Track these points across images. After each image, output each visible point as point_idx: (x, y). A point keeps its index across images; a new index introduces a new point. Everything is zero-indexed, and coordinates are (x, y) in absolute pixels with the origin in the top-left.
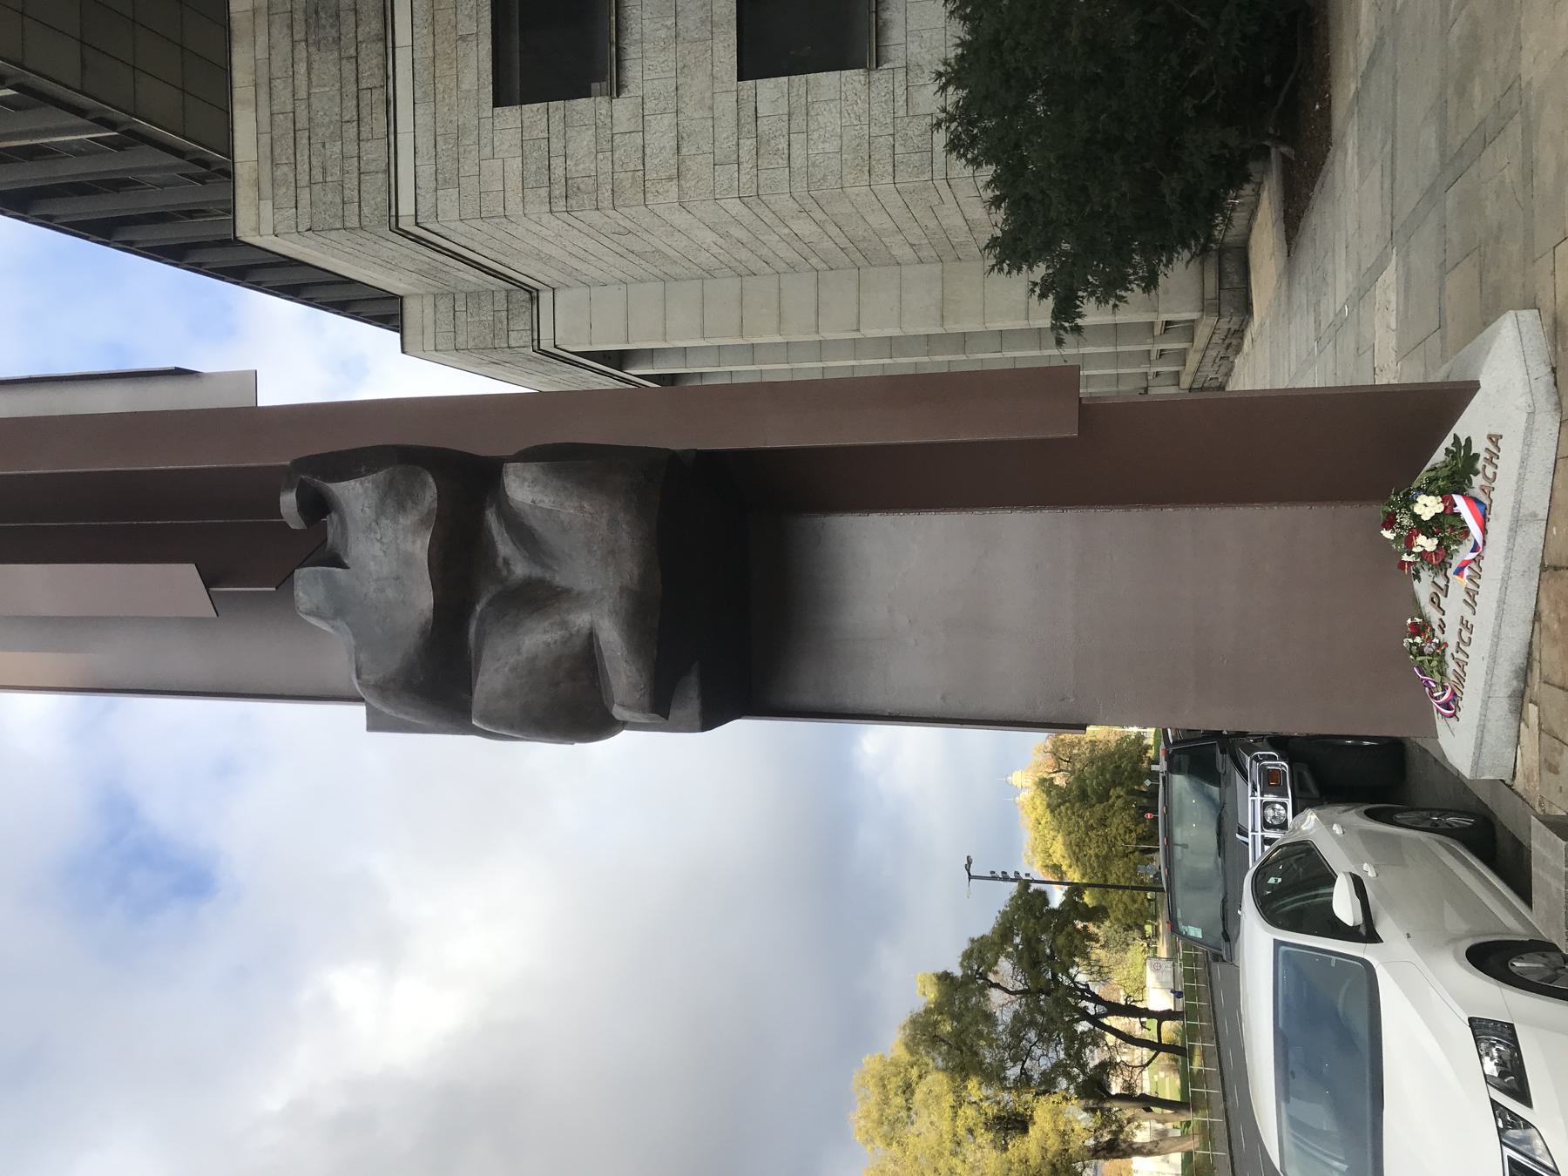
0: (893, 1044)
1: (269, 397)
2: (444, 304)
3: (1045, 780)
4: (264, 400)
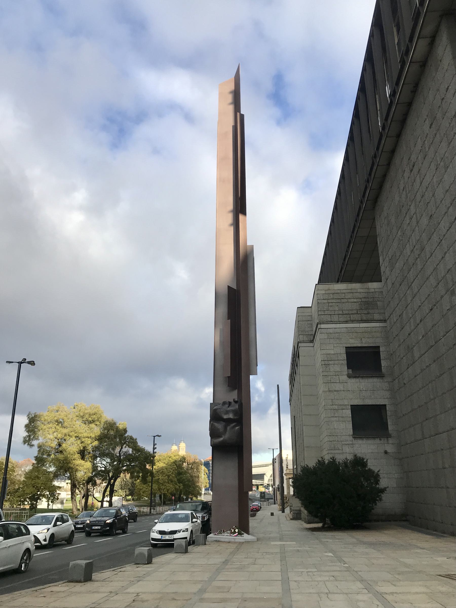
0: (108, 415)
2: (309, 318)
3: (185, 460)
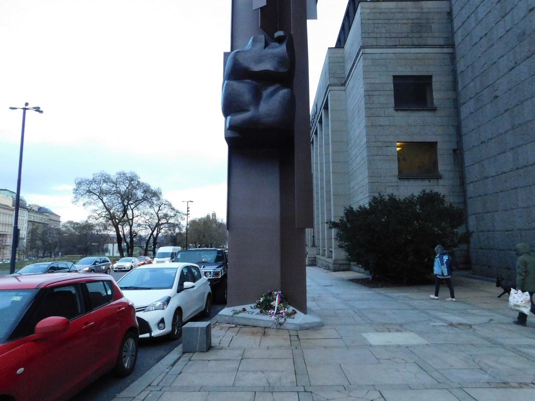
1: (309, 23)
4: (308, 21)
